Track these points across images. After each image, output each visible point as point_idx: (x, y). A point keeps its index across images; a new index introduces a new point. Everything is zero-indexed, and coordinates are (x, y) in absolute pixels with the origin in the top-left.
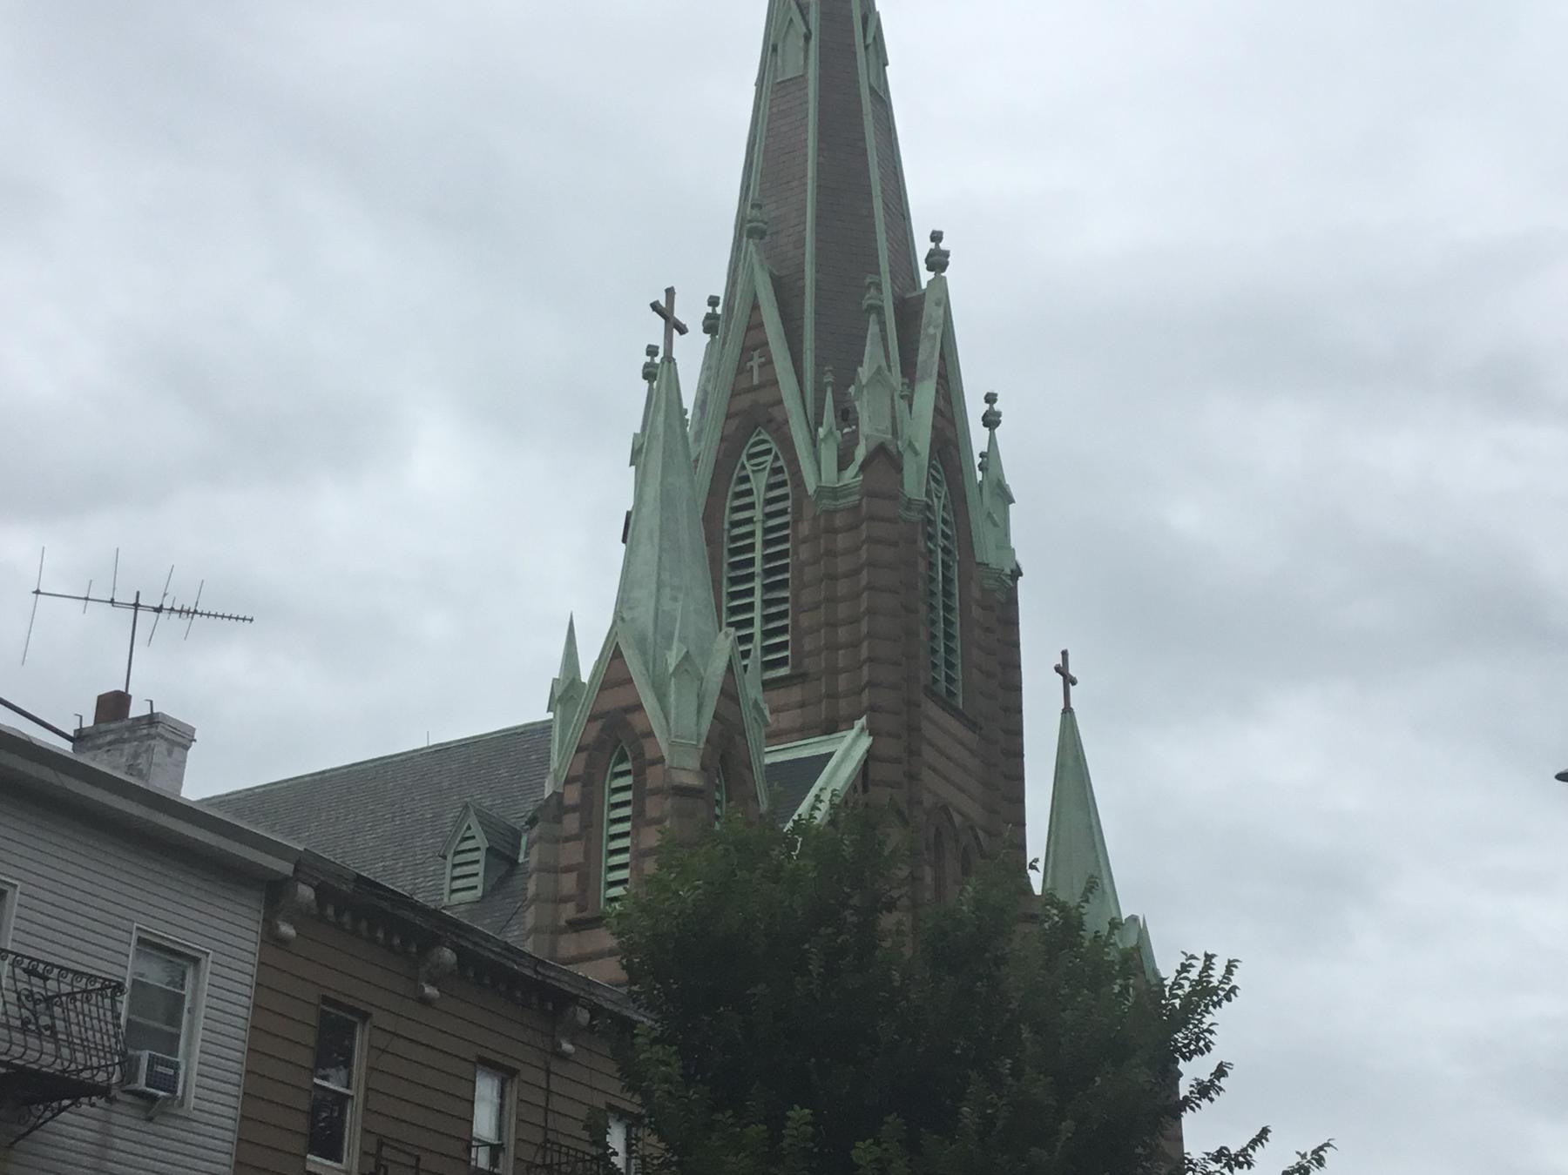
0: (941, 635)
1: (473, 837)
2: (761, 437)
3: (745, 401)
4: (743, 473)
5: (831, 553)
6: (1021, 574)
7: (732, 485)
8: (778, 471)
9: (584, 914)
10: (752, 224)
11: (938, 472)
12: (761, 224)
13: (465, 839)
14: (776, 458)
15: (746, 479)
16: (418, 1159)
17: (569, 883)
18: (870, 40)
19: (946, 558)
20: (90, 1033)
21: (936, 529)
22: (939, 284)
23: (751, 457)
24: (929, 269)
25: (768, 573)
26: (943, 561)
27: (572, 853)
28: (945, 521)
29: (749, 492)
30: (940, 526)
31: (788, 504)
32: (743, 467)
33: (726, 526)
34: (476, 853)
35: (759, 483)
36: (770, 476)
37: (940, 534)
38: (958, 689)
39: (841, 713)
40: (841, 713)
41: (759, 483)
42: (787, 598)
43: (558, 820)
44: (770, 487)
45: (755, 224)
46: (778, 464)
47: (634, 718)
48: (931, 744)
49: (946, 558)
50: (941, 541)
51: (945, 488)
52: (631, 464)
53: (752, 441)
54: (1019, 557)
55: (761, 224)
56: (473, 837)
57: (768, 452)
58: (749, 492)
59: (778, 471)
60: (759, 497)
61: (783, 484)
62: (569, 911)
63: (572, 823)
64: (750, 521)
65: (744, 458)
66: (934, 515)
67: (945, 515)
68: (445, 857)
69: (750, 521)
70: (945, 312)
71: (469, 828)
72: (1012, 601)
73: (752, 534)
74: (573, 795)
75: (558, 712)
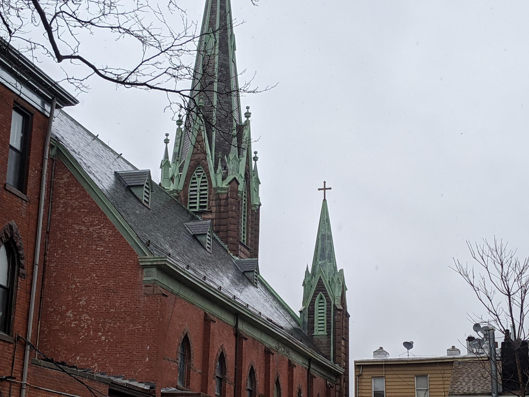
2: (199, 168)
4: (194, 177)
6: (261, 205)
7: (190, 184)
8: (205, 178)
12: (203, 105)
14: (204, 174)
15: (195, 179)
18: (232, 45)
22: (247, 123)
23: (197, 172)
24: (246, 117)
31: (206, 204)
36: (202, 179)
41: (199, 180)
42: (206, 201)
44: (202, 182)
46: (204, 176)
52: (160, 168)
53: (197, 168)
54: (261, 201)
55: (203, 105)
57: (202, 172)
58: (196, 183)
59: (205, 178)
61: (206, 182)
65: (195, 173)
69: (196, 191)
70: (342, 295)
72: (258, 213)
75: (163, 169)
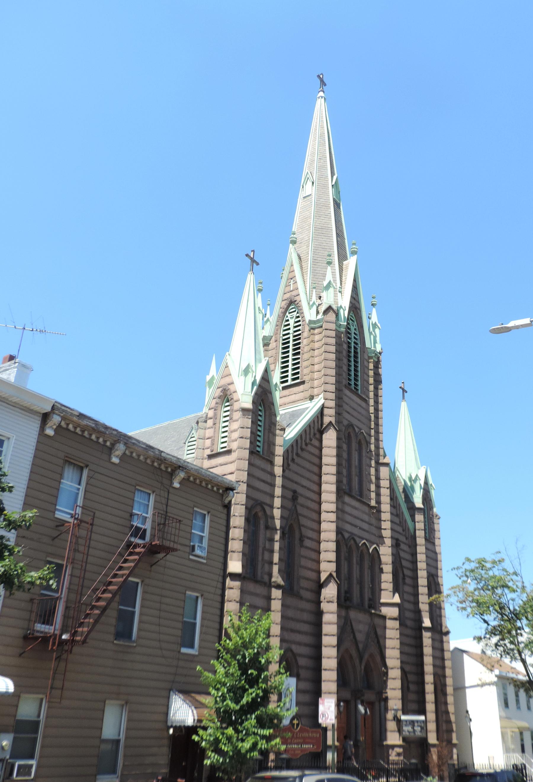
0: (353, 370)
1: (194, 437)
3: (287, 296)
4: (287, 319)
5: (313, 341)
9: (213, 453)
10: (292, 239)
11: (352, 317)
13: (191, 438)
15: (288, 320)
16: (94, 513)
17: (208, 443)
19: (355, 345)
20: (173, 536)
21: (351, 336)
23: (290, 313)
25: (288, 347)
26: (354, 346)
27: (209, 433)
28: (355, 333)
29: (289, 325)
30: (353, 335)
32: (287, 317)
33: (281, 335)
34: (195, 442)
35: (292, 322)
37: (353, 337)
38: (359, 388)
39: (315, 393)
40: (315, 393)
41: (292, 322)
43: (206, 422)
45: (292, 239)
47: (230, 387)
48: (347, 404)
49: (355, 345)
50: (353, 340)
51: (356, 323)
56: (194, 437)
58: (289, 325)
59: (298, 317)
60: (291, 326)
62: (208, 452)
63: (210, 423)
64: (289, 334)
66: (351, 331)
67: (355, 332)
68: (185, 443)
69: (289, 334)
71: (193, 434)
73: (289, 338)
74: (211, 413)
